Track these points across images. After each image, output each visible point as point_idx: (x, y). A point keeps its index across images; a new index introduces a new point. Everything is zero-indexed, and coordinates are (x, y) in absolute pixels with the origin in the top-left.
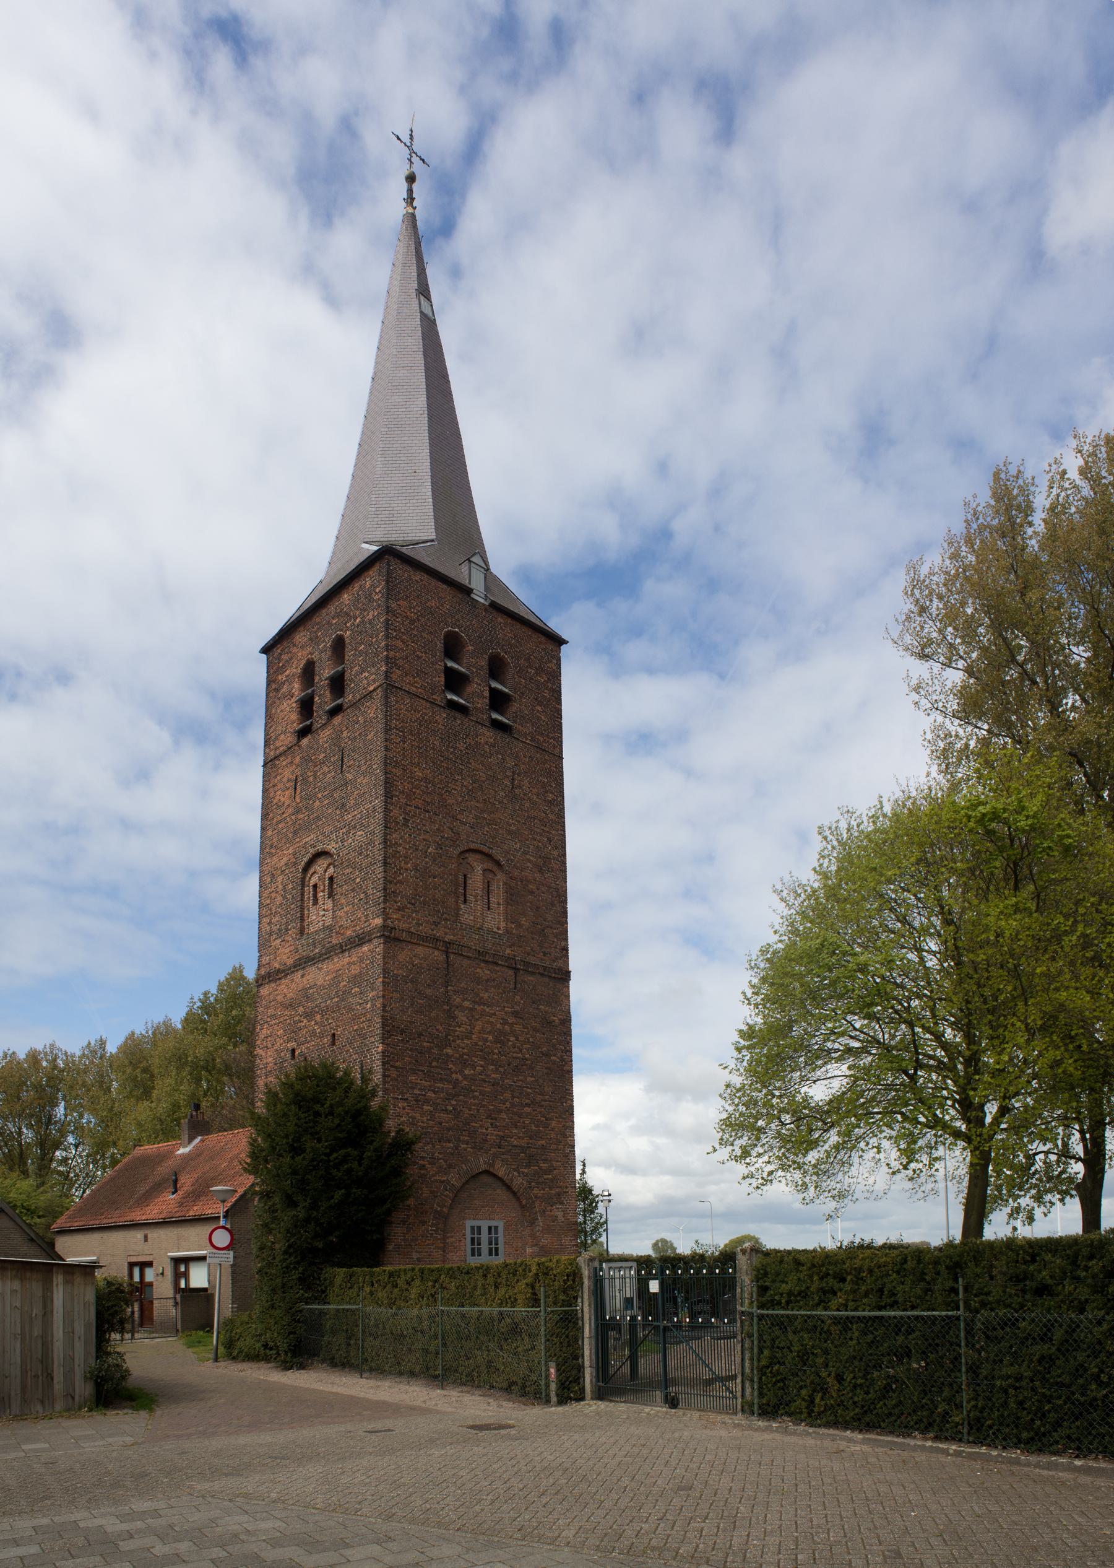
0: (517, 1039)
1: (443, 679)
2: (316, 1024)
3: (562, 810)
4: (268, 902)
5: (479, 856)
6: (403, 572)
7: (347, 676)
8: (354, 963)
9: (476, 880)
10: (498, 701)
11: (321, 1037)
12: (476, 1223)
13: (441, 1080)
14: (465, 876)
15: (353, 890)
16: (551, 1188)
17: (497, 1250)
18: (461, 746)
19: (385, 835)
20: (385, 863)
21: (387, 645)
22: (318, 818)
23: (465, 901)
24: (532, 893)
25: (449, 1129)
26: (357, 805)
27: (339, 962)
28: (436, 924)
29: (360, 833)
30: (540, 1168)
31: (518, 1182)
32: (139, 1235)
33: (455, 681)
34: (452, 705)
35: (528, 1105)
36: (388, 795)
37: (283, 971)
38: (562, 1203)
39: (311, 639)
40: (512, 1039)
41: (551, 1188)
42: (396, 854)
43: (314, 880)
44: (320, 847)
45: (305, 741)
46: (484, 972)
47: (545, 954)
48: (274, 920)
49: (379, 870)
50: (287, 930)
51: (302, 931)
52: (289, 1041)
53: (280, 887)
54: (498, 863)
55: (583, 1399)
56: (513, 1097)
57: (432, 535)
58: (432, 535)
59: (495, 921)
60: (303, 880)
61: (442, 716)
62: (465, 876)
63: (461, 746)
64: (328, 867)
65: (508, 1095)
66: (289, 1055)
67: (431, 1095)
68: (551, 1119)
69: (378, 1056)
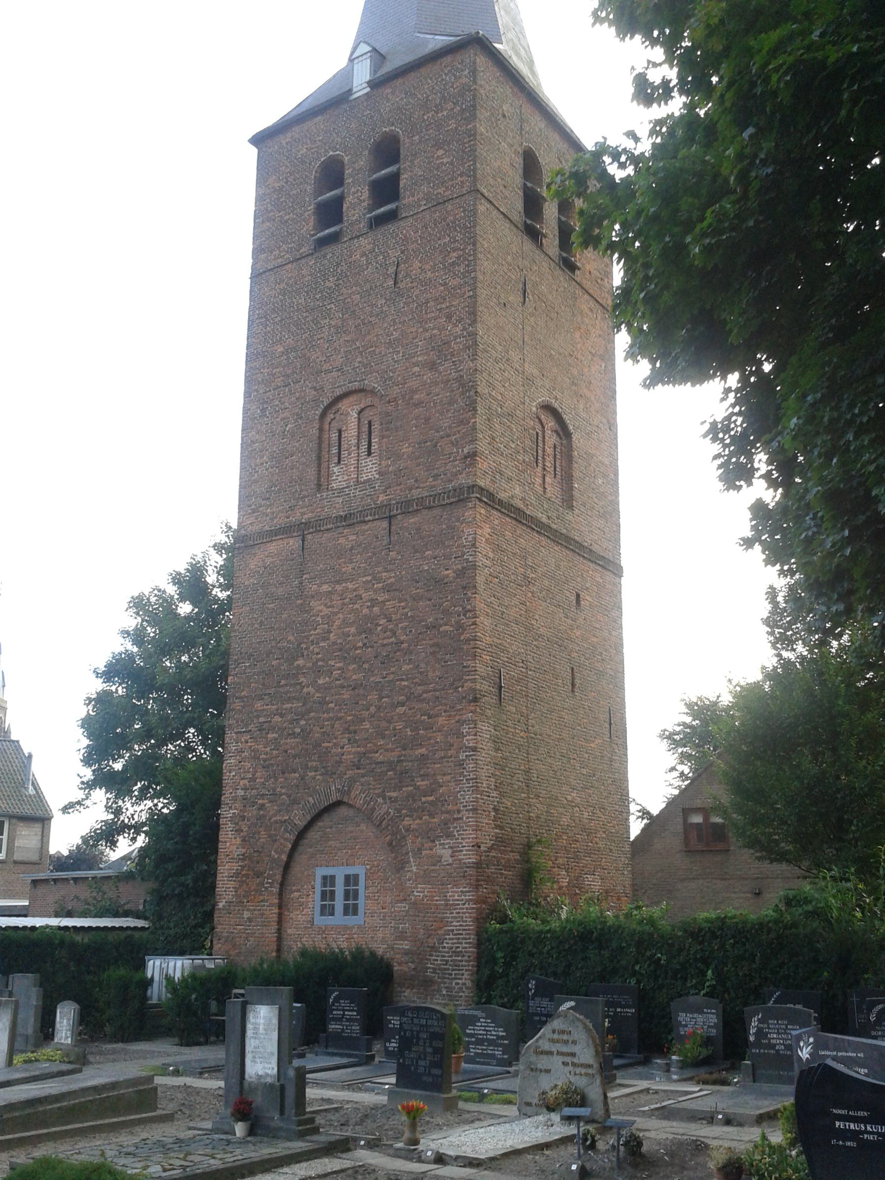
12: (329, 871)
14: (340, 432)
16: (432, 815)
17: (356, 907)
25: (295, 757)
30: (417, 788)
38: (449, 835)
40: (382, 622)
41: (432, 815)
47: (436, 477)
55: (334, 891)
56: (381, 698)
62: (340, 432)
65: (373, 697)
67: (277, 719)
68: (438, 715)
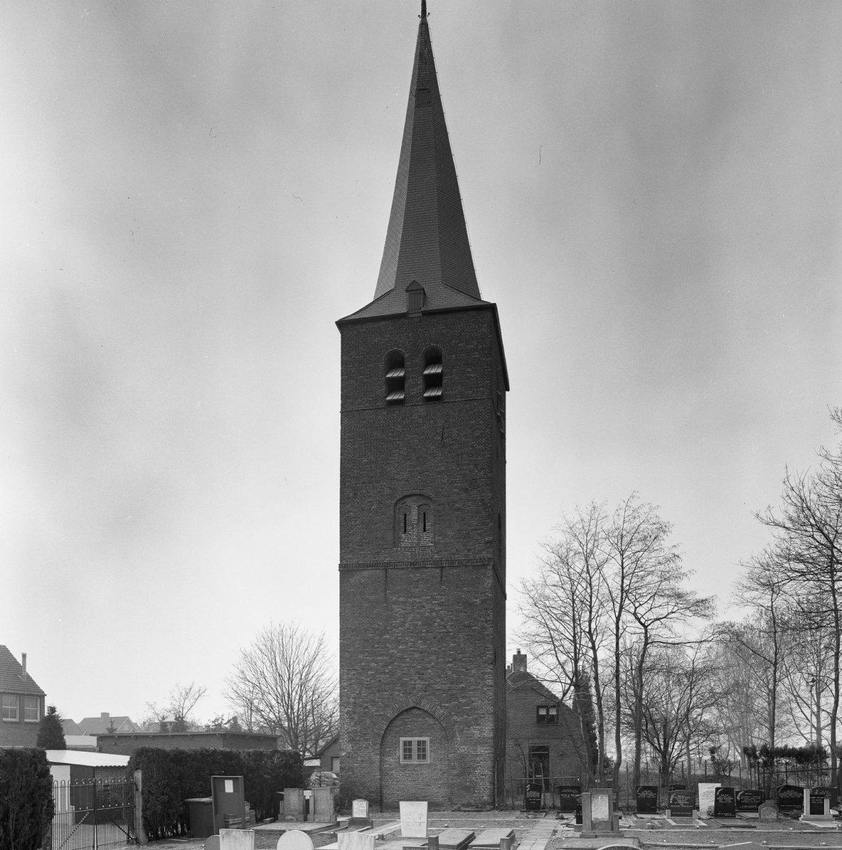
0: (442, 620)
5: (415, 498)
9: (414, 516)
14: (405, 515)
28: (378, 553)
35: (451, 662)
47: (469, 550)
54: (429, 498)
57: (700, 785)
58: (700, 785)
62: (405, 515)
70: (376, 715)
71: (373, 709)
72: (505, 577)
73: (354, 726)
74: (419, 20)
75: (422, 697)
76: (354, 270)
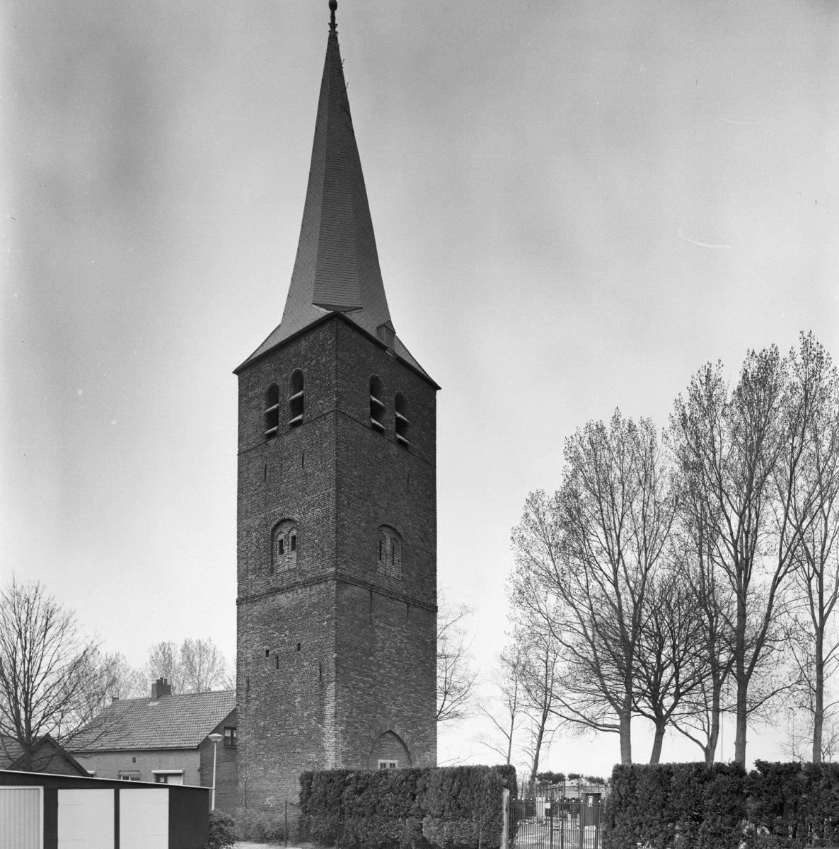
1: (369, 409)
2: (286, 636)
3: (435, 501)
4: (245, 549)
5: (388, 529)
6: (346, 331)
7: (305, 400)
8: (313, 595)
9: (388, 546)
10: (401, 426)
11: (290, 644)
13: (367, 676)
14: (380, 542)
15: (312, 547)
16: (424, 742)
18: (380, 456)
19: (337, 513)
20: (337, 532)
21: (337, 383)
22: (284, 496)
23: (380, 559)
24: (417, 555)
25: (371, 706)
26: (315, 491)
27: (301, 594)
29: (318, 510)
31: (406, 738)
32: (129, 758)
33: (376, 411)
34: (374, 426)
35: (413, 692)
36: (338, 487)
37: (258, 596)
39: (275, 370)
41: (424, 742)
42: (343, 526)
43: (281, 537)
44: (286, 516)
45: (272, 442)
46: (391, 605)
47: (424, 594)
48: (250, 562)
49: (332, 536)
50: (260, 569)
51: (272, 571)
52: (264, 644)
53: (254, 540)
54: (399, 535)
56: (405, 687)
59: (395, 572)
60: (272, 536)
61: (369, 434)
62: (380, 542)
63: (380, 456)
64: (291, 530)
66: (264, 653)
67: (361, 684)
69: (332, 660)
70: (364, 736)
71: (362, 730)
72: (57, 827)
73: (347, 746)
74: (329, 28)
75: (395, 722)
76: (251, 294)
